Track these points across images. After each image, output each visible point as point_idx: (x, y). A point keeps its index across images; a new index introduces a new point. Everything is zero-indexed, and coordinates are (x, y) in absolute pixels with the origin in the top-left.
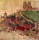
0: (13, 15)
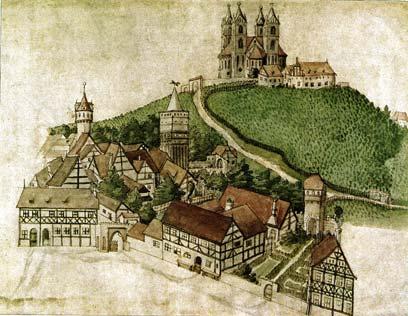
0: (142, 119)
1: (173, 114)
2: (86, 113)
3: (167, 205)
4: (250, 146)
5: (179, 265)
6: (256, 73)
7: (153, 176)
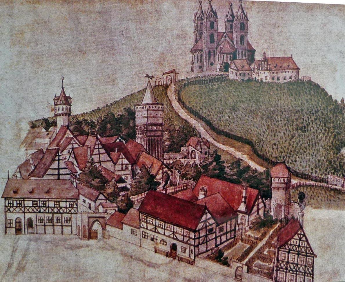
0: (118, 112)
1: (148, 107)
2: (64, 106)
3: (144, 195)
4: (222, 138)
5: (156, 252)
6: (226, 67)
7: (130, 167)
